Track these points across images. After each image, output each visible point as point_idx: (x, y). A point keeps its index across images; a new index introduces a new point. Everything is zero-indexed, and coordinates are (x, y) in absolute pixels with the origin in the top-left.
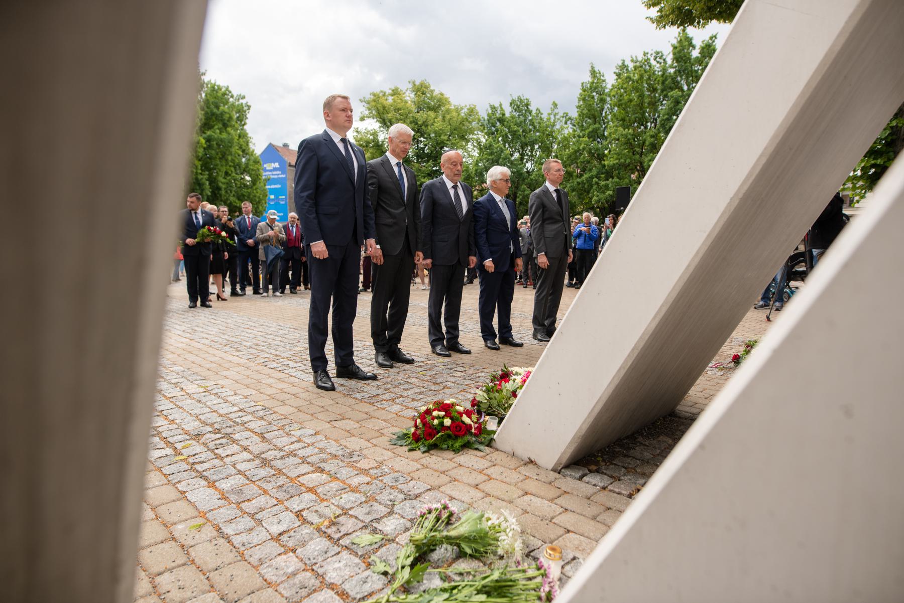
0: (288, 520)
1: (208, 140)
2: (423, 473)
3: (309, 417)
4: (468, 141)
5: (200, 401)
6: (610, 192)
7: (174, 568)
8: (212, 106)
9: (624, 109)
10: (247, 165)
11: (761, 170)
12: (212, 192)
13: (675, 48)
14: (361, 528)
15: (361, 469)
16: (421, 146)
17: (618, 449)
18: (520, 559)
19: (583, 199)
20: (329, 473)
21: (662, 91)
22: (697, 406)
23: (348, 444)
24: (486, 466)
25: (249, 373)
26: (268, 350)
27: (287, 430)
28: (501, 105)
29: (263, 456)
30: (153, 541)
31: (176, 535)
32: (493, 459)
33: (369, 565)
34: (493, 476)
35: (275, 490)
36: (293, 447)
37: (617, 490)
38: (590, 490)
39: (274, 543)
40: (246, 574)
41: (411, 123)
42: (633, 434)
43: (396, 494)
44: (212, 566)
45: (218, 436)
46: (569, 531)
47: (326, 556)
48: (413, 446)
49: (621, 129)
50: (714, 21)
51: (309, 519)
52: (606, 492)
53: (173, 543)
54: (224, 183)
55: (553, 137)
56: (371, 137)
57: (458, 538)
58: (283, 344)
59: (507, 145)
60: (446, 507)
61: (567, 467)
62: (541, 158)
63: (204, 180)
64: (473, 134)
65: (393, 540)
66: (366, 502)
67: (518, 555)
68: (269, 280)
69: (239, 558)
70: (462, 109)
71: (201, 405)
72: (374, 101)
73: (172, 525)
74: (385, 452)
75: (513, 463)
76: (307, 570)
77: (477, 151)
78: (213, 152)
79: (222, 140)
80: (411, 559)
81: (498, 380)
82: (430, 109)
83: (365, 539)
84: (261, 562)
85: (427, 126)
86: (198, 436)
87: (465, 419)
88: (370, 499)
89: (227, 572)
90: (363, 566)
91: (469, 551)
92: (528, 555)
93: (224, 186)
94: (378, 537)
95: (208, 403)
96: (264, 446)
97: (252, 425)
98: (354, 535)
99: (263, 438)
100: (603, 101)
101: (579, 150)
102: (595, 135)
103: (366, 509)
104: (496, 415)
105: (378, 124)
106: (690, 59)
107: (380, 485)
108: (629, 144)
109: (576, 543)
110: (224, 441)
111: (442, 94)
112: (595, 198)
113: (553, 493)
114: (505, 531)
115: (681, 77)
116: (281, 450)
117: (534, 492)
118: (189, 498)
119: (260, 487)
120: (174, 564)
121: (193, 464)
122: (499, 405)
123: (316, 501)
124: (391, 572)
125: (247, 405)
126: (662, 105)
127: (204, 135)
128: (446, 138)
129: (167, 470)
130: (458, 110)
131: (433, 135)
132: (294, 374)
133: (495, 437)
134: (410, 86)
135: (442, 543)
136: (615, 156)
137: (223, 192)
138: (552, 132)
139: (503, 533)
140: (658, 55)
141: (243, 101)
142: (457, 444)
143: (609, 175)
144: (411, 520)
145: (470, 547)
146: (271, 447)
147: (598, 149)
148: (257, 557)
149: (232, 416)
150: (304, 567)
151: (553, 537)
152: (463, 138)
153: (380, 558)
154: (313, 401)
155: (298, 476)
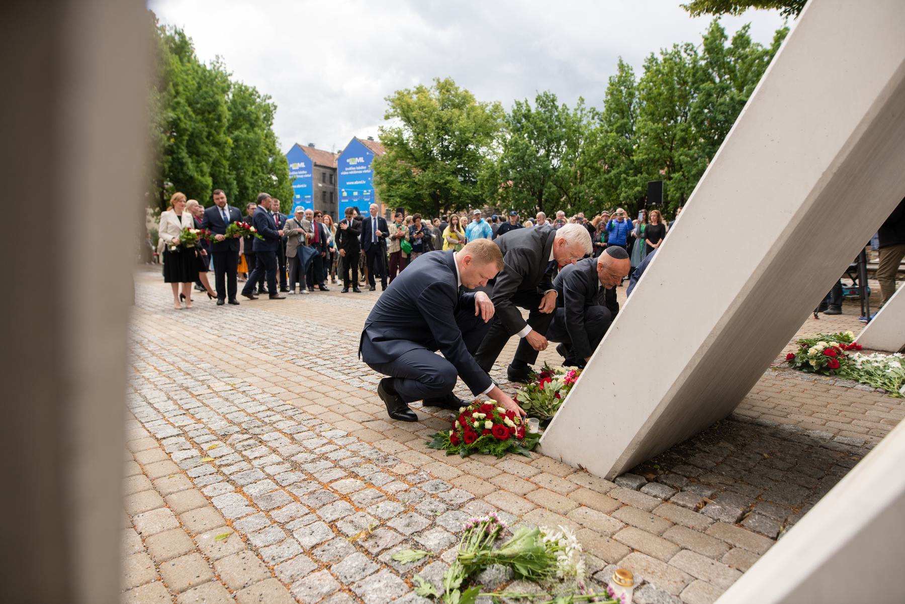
0: (321, 531)
1: (236, 140)
2: (465, 480)
3: (340, 417)
4: (492, 138)
5: (227, 400)
6: (639, 188)
7: (198, 584)
8: (240, 107)
9: (653, 103)
10: (274, 164)
11: (861, 139)
12: (240, 192)
13: (706, 39)
14: (401, 543)
15: (397, 475)
16: (446, 143)
17: (675, 456)
18: (583, 583)
19: (611, 196)
20: (363, 479)
21: (693, 84)
22: (755, 408)
23: (381, 447)
24: (533, 473)
25: (277, 370)
26: (296, 347)
27: (317, 431)
28: (526, 101)
29: (293, 458)
30: (176, 552)
31: (202, 546)
32: (540, 466)
33: (412, 586)
34: (541, 485)
35: (306, 497)
36: (324, 449)
37: (681, 503)
38: (650, 502)
39: (307, 558)
40: (276, 594)
41: (435, 121)
42: (689, 439)
43: (437, 503)
44: (239, 583)
45: (246, 436)
46: (633, 550)
47: (364, 574)
48: (452, 450)
49: (650, 123)
50: (752, 8)
51: (344, 530)
52: (669, 505)
53: (197, 555)
54: (251, 183)
55: (579, 133)
56: (396, 136)
57: (512, 557)
58: (311, 341)
59: (533, 142)
60: (494, 521)
61: (622, 475)
62: (567, 154)
63: (232, 180)
64: (498, 131)
65: (438, 557)
66: (405, 512)
67: (581, 578)
68: (296, 278)
69: (269, 574)
70: (487, 105)
71: (228, 404)
72: (399, 99)
73: (197, 534)
74: (422, 456)
75: (562, 471)
76: (344, 590)
77: (502, 148)
78: (241, 152)
79: (249, 140)
80: (460, 580)
81: (539, 380)
82: (455, 106)
83: (406, 554)
84: (293, 579)
85: (451, 124)
86: (225, 437)
87: (507, 421)
88: (409, 509)
89: (255, 590)
90: (406, 587)
91: (524, 572)
92: (591, 579)
93: (251, 186)
94: (421, 553)
95: (236, 402)
96: (294, 448)
97: (281, 426)
98: (394, 550)
99: (293, 439)
100: (631, 95)
101: (606, 145)
102: (623, 130)
103: (404, 520)
104: (539, 418)
105: (403, 123)
106: (721, 50)
107: (419, 492)
108: (658, 138)
109: (644, 564)
110: (251, 442)
111: (467, 92)
112: (623, 194)
113: (610, 505)
114: (563, 549)
115: (713, 69)
116: (311, 452)
117: (588, 503)
118: (215, 504)
119: (290, 493)
120: (197, 580)
121: (220, 466)
122: (542, 407)
123: (350, 510)
124: (438, 595)
125: (275, 404)
126: (693, 98)
127: (232, 136)
128: (471, 135)
129: (192, 473)
130: (483, 108)
131: (457, 133)
132: (323, 372)
133: (540, 441)
134: (435, 84)
135: (494, 562)
136: (644, 151)
137: (250, 192)
138: (579, 127)
139: (560, 552)
140: (689, 47)
141: (269, 102)
142: (500, 449)
143: (637, 171)
144: (456, 534)
145: (526, 568)
146: (301, 449)
147: (626, 145)
148: (288, 573)
149: (260, 415)
150: (339, 586)
151: (616, 556)
152: (487, 135)
153: (425, 578)
154: (344, 401)
155: (331, 482)
